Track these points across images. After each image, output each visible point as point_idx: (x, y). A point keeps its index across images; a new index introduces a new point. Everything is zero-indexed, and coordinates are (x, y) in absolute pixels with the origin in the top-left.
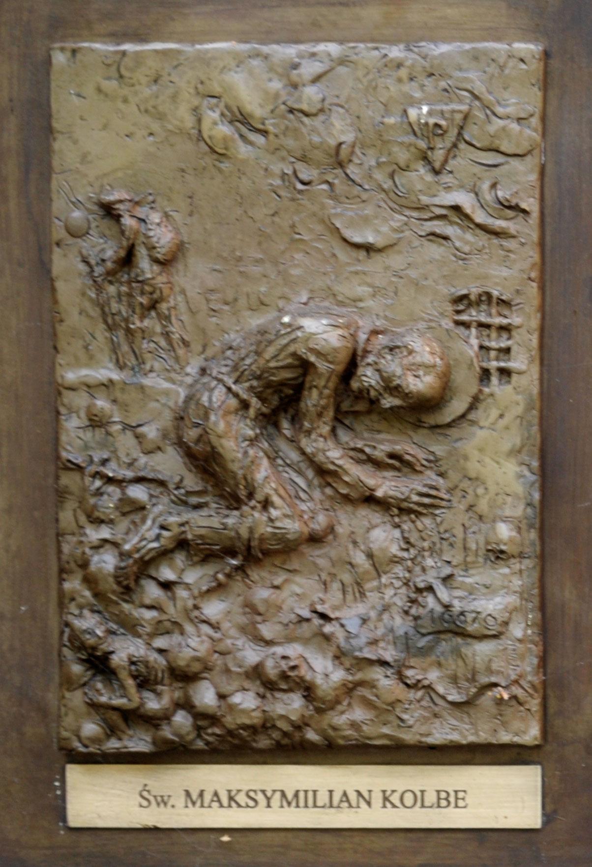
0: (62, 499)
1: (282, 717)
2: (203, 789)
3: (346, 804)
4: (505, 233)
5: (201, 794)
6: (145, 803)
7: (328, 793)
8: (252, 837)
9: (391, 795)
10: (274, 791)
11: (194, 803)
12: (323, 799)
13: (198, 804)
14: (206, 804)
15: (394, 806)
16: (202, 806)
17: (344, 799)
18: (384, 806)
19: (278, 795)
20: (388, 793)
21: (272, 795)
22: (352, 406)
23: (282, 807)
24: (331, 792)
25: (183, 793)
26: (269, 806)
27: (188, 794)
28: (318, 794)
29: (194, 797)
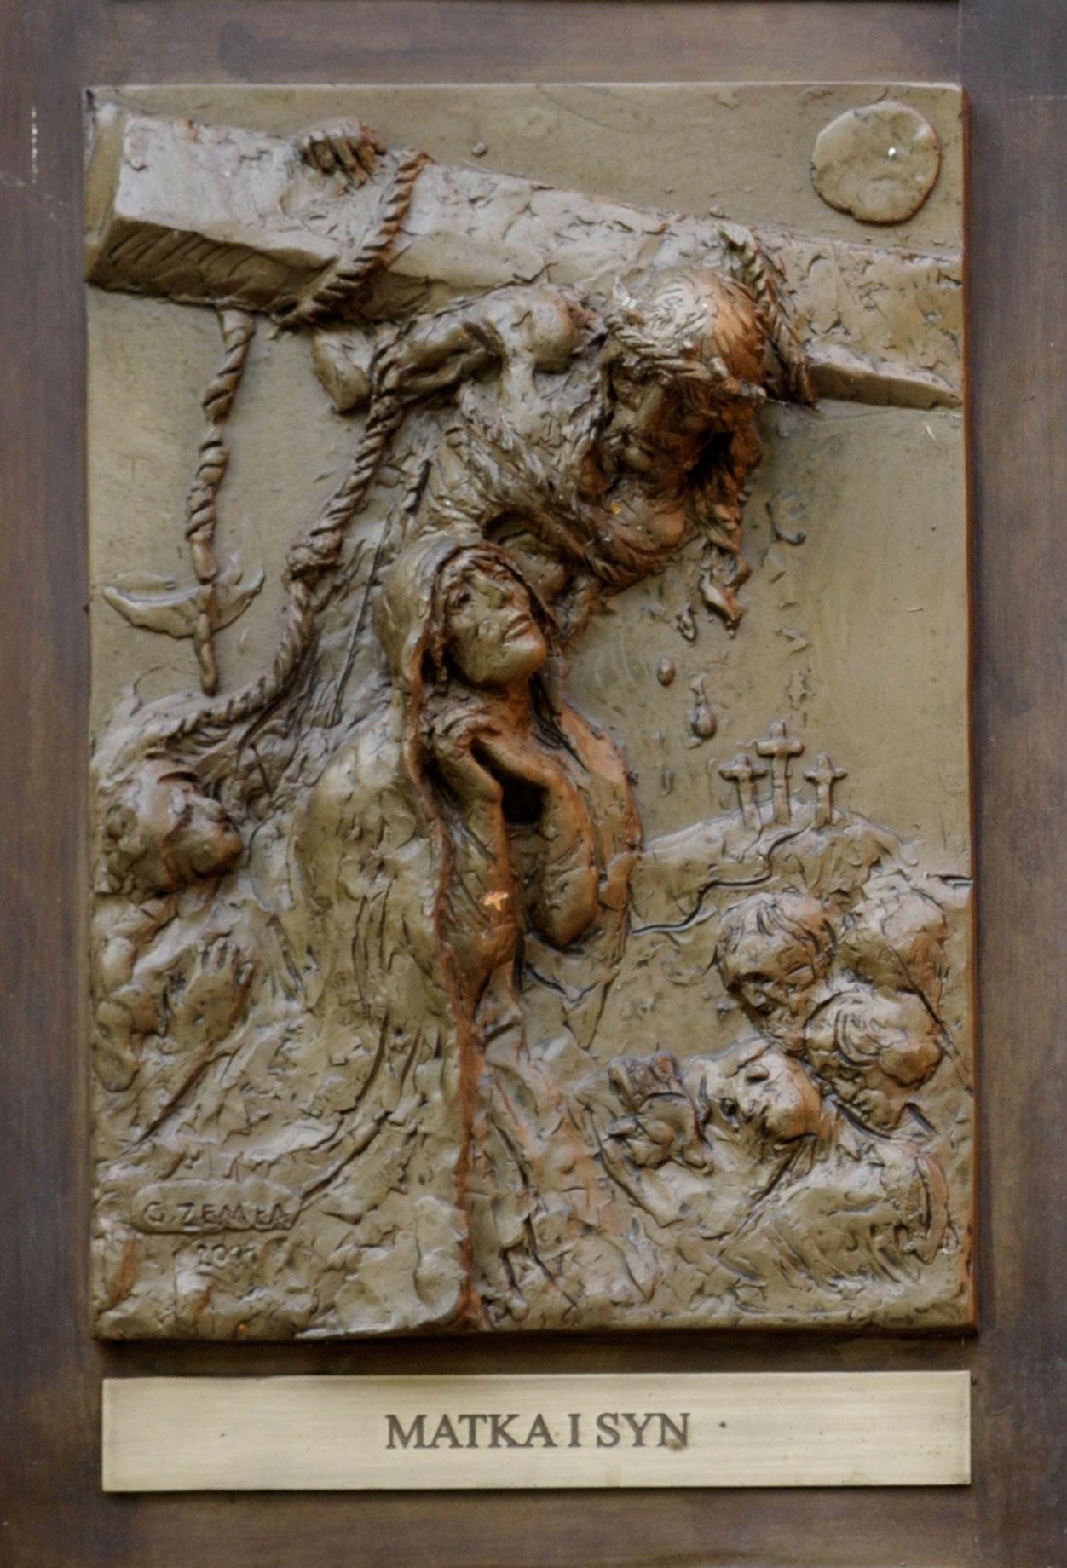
0: (841, 1018)
1: (940, 1293)
2: (422, 1413)
3: (448, 1441)
4: (90, 977)
5: (419, 1421)
6: (608, 1439)
7: (569, 1420)
8: (374, 1509)
9: (506, 1423)
10: (649, 1416)
11: (405, 1441)
12: (653, 1432)
13: (414, 1440)
14: (428, 1440)
15: (456, 1444)
16: (420, 1444)
17: (444, 1431)
18: (495, 1444)
19: (657, 1421)
20: (501, 1421)
21: (646, 1423)
22: (829, 1025)
23: (391, 1445)
24: (575, 1418)
25: (387, 1421)
26: (639, 1442)
27: (394, 1422)
28: (426, 1422)
29: (406, 1429)
